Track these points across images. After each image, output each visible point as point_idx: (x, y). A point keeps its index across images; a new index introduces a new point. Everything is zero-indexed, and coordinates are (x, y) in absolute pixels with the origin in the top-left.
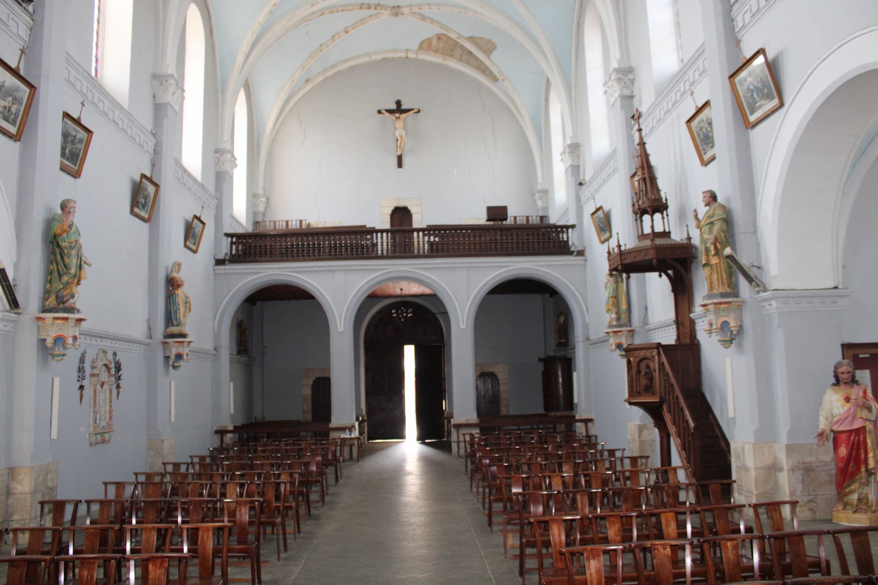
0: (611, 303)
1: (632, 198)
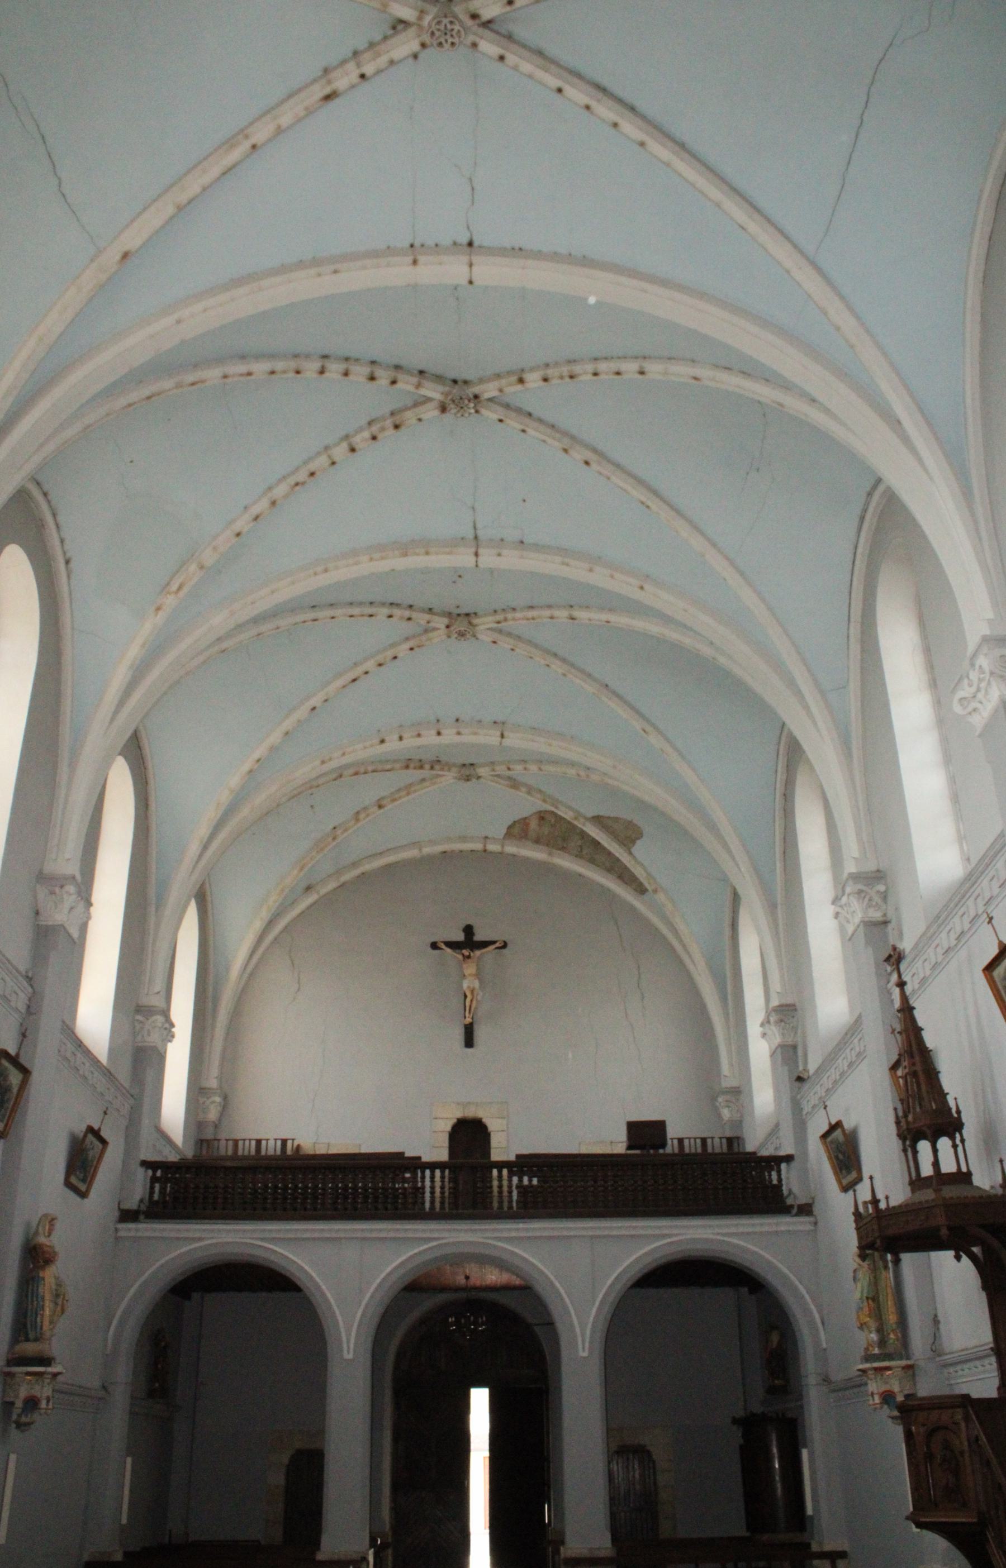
0: (866, 1310)
1: (895, 1109)
